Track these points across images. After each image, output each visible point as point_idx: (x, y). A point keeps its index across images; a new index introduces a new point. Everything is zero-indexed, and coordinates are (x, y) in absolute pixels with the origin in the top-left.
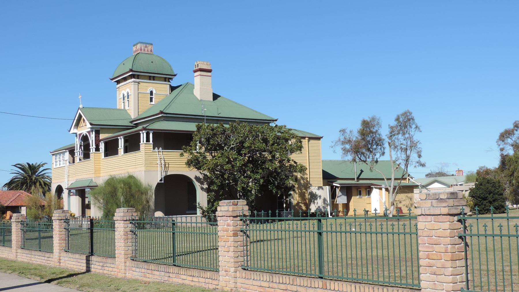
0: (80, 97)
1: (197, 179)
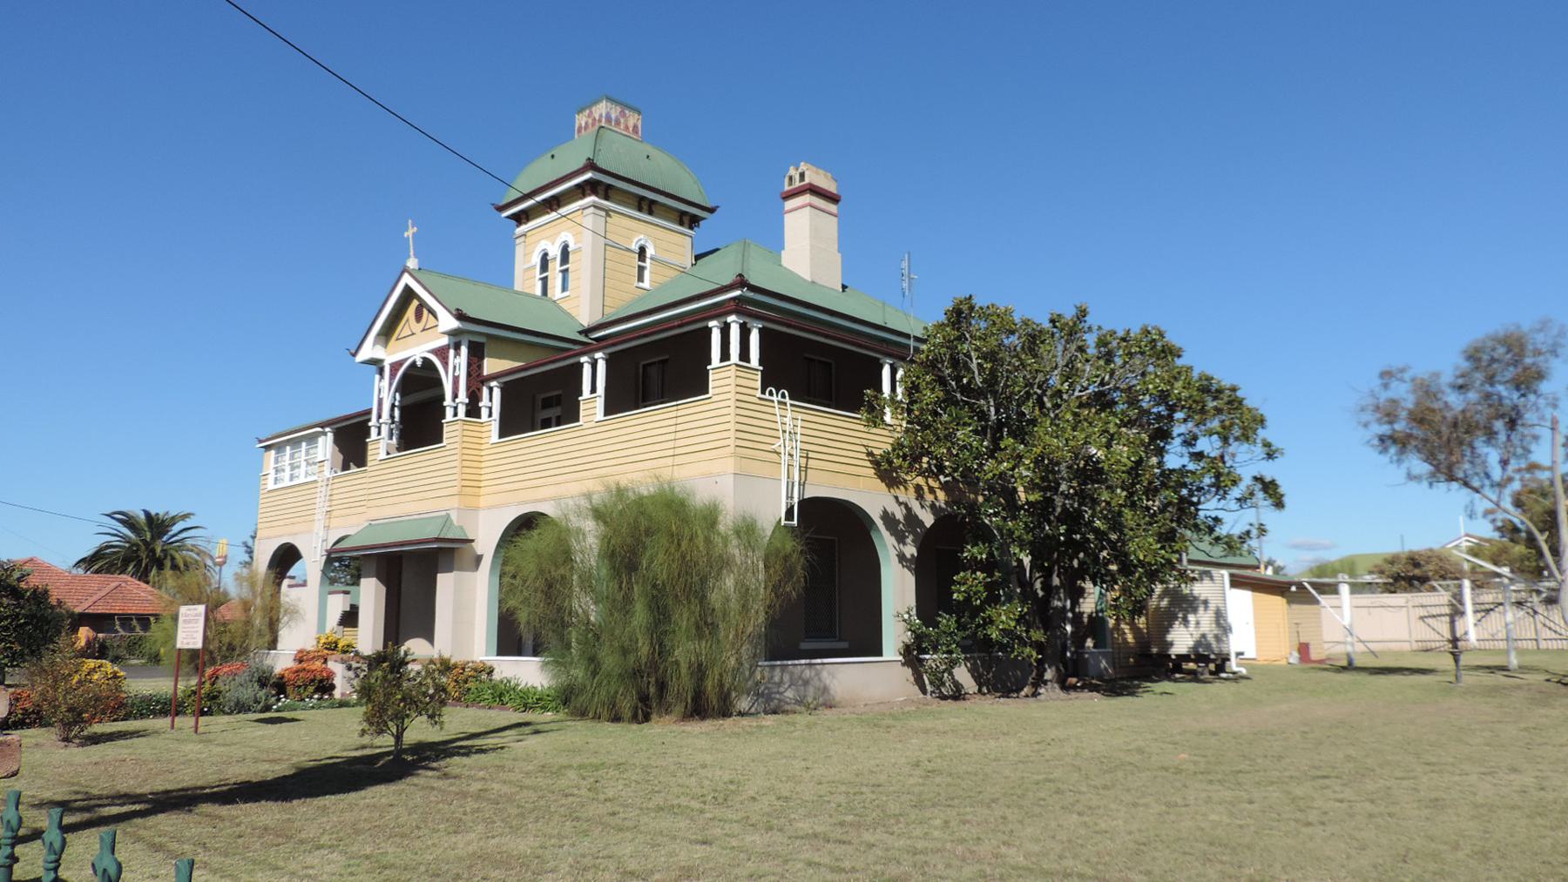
0: (409, 233)
1: (888, 518)
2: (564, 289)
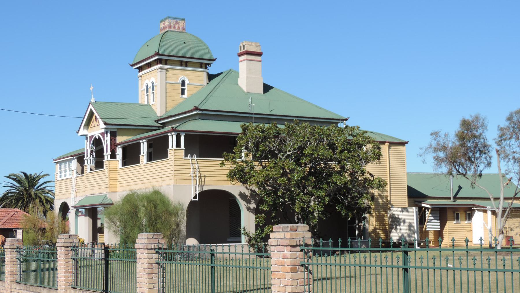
0: (91, 89)
1: (243, 196)
2: (154, 101)
